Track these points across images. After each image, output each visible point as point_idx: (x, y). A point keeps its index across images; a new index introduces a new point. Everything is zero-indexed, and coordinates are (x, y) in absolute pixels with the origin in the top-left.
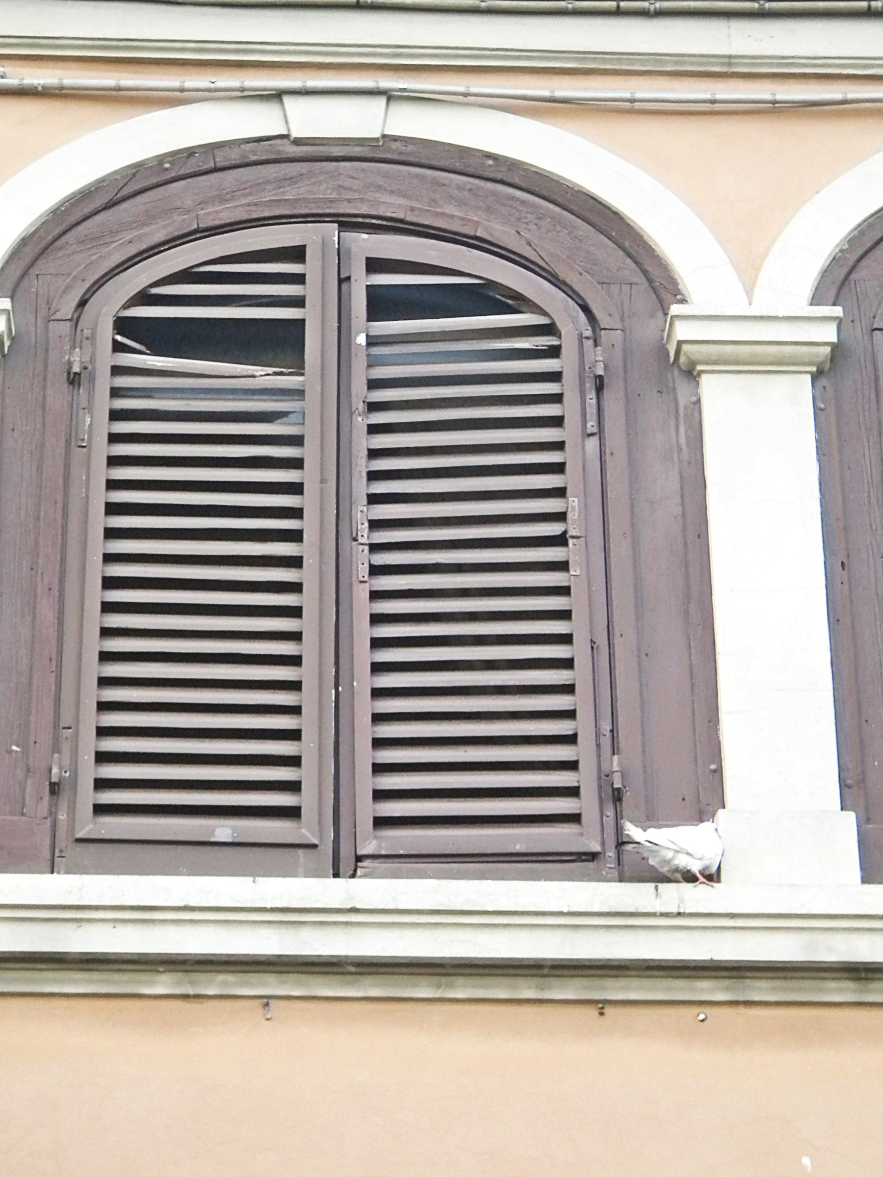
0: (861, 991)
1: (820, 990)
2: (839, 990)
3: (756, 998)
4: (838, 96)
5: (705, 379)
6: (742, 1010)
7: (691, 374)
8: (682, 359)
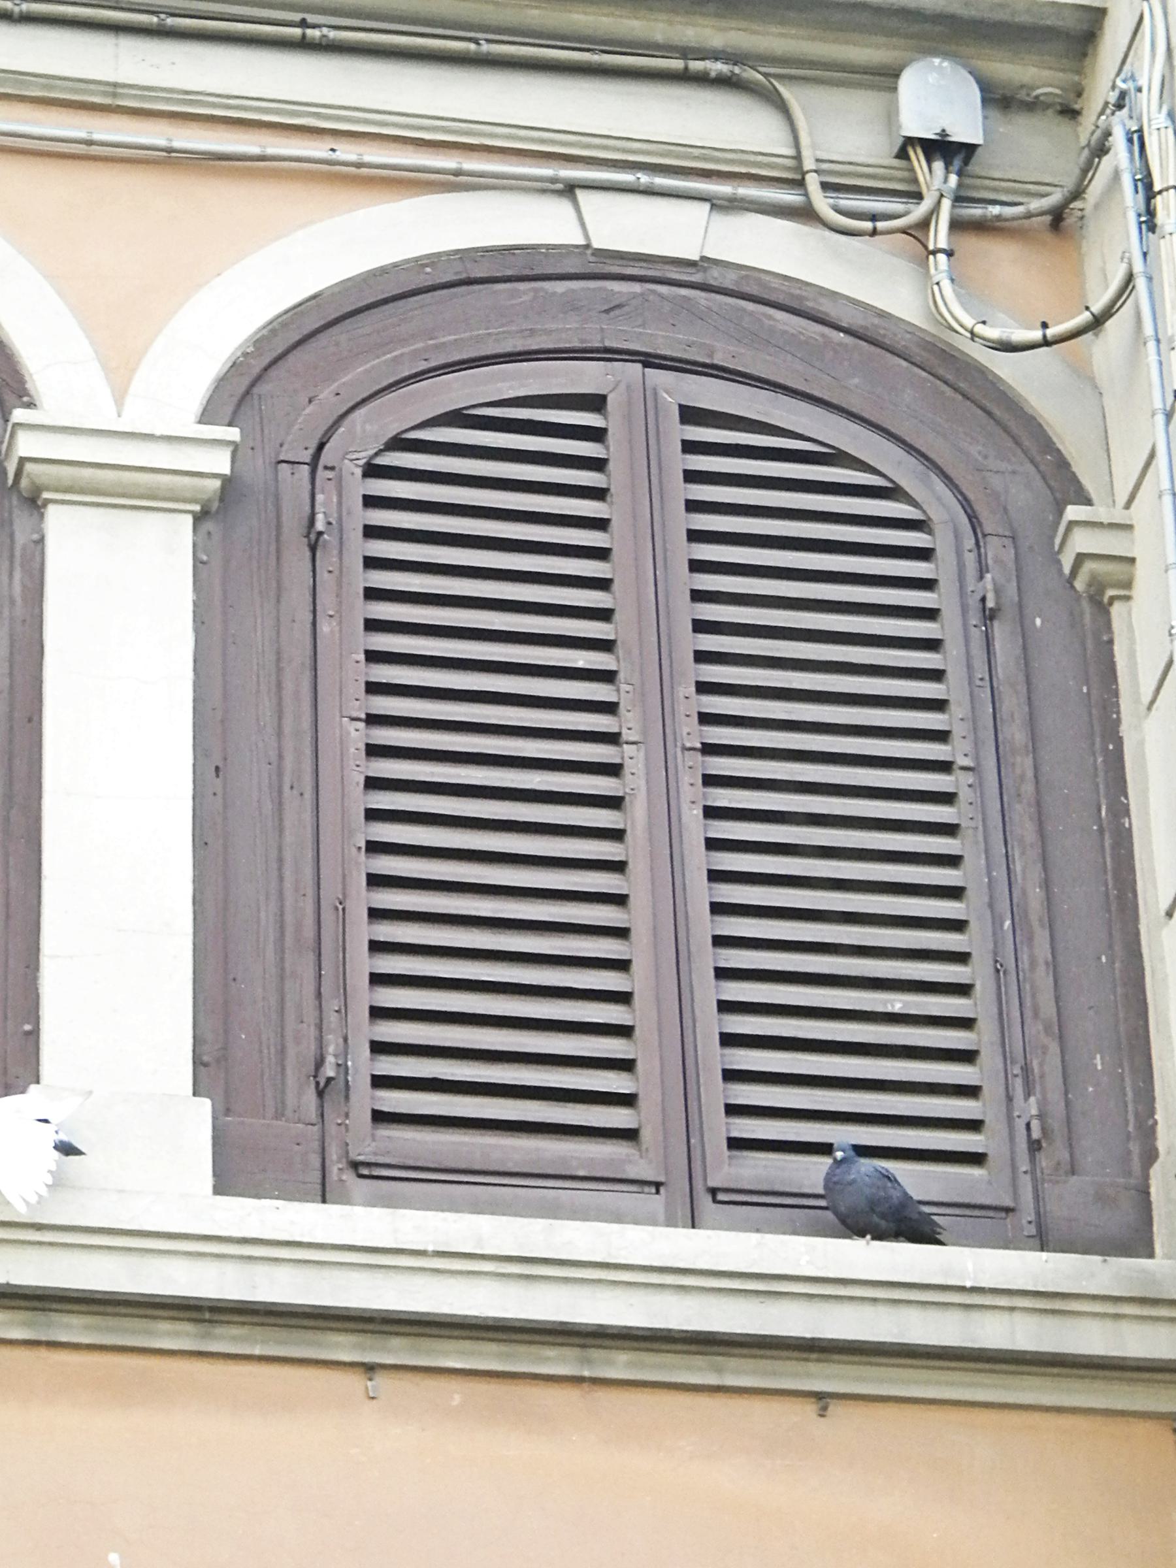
0: (205, 1336)
1: (150, 1333)
2: (177, 1334)
3: (64, 1338)
4: (255, 150)
5: (52, 511)
6: (43, 1353)
7: (35, 503)
8: (24, 483)
